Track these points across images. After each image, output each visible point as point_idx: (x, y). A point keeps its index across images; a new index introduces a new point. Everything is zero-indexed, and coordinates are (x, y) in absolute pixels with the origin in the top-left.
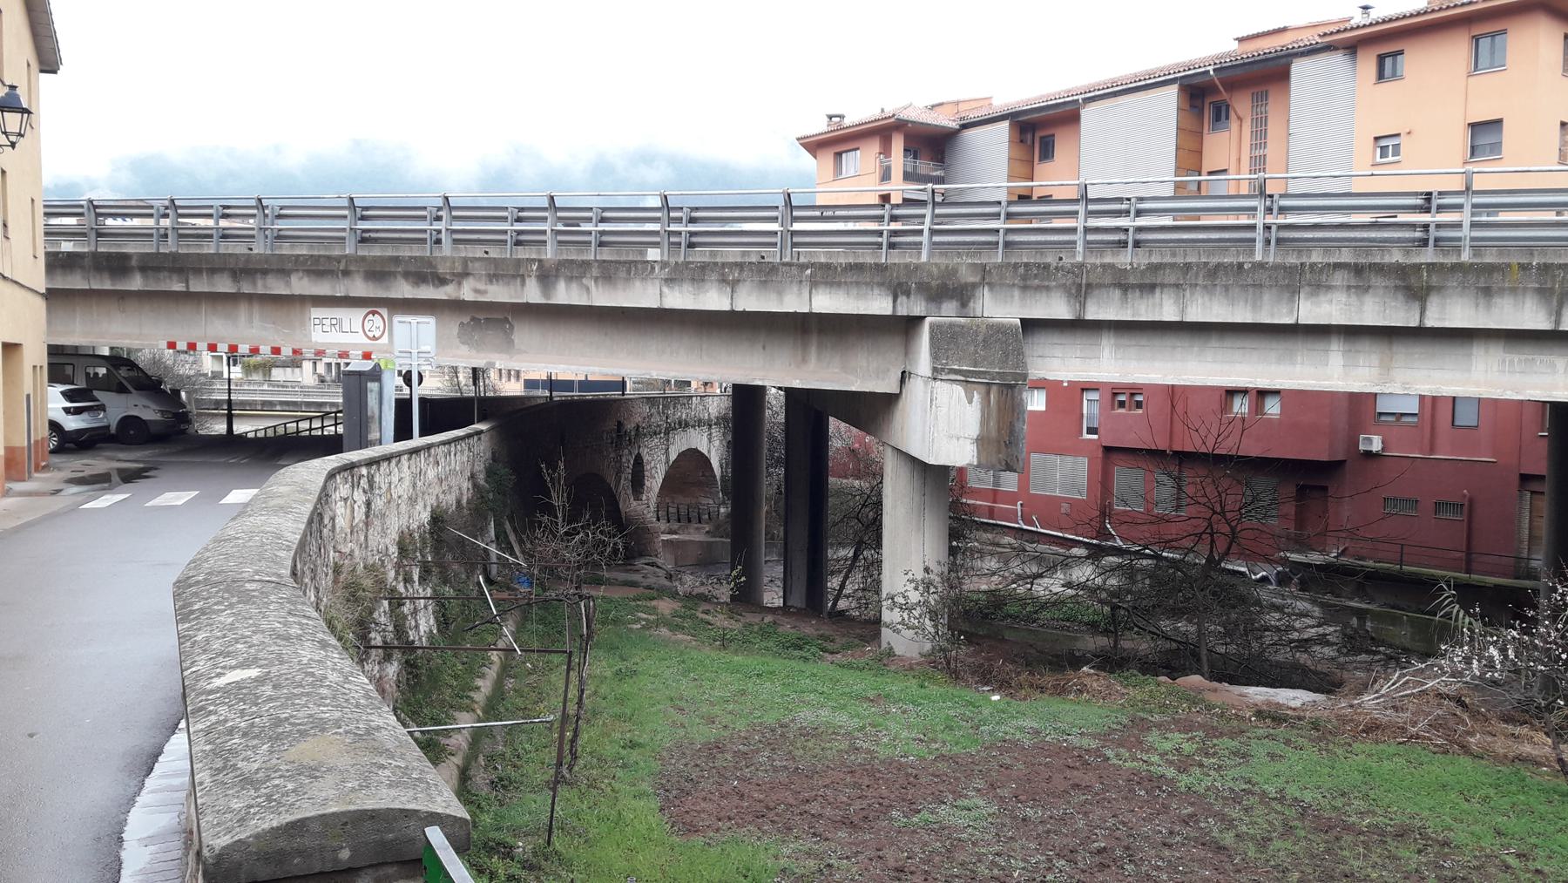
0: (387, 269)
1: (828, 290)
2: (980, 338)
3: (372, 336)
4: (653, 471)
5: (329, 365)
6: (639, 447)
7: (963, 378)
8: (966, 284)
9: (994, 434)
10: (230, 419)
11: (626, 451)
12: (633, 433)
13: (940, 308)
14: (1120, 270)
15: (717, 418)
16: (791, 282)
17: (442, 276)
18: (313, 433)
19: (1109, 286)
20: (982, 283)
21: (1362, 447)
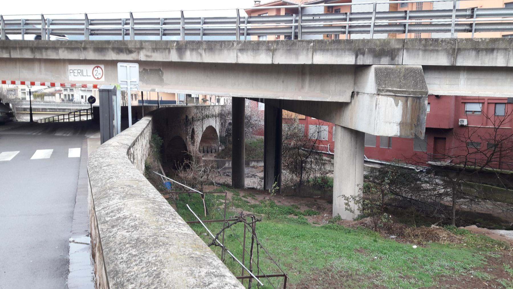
0: (104, 47)
1: (322, 53)
2: (402, 75)
3: (97, 78)
5: (65, 95)
6: (193, 125)
7: (393, 94)
8: (394, 49)
9: (409, 121)
10: (31, 115)
11: (189, 127)
12: (191, 120)
13: (380, 61)
14: (476, 42)
15: (218, 114)
16: (303, 49)
17: (130, 49)
18: (65, 120)
19: (469, 50)
20: (403, 48)
21: (460, 124)
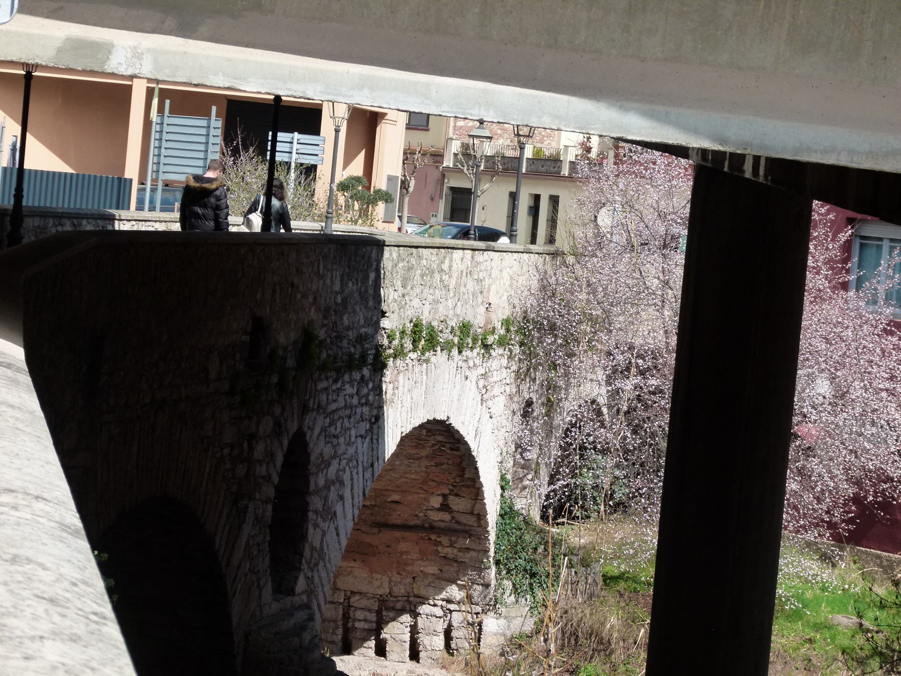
4: (333, 496)
11: (267, 424)
15: (507, 323)
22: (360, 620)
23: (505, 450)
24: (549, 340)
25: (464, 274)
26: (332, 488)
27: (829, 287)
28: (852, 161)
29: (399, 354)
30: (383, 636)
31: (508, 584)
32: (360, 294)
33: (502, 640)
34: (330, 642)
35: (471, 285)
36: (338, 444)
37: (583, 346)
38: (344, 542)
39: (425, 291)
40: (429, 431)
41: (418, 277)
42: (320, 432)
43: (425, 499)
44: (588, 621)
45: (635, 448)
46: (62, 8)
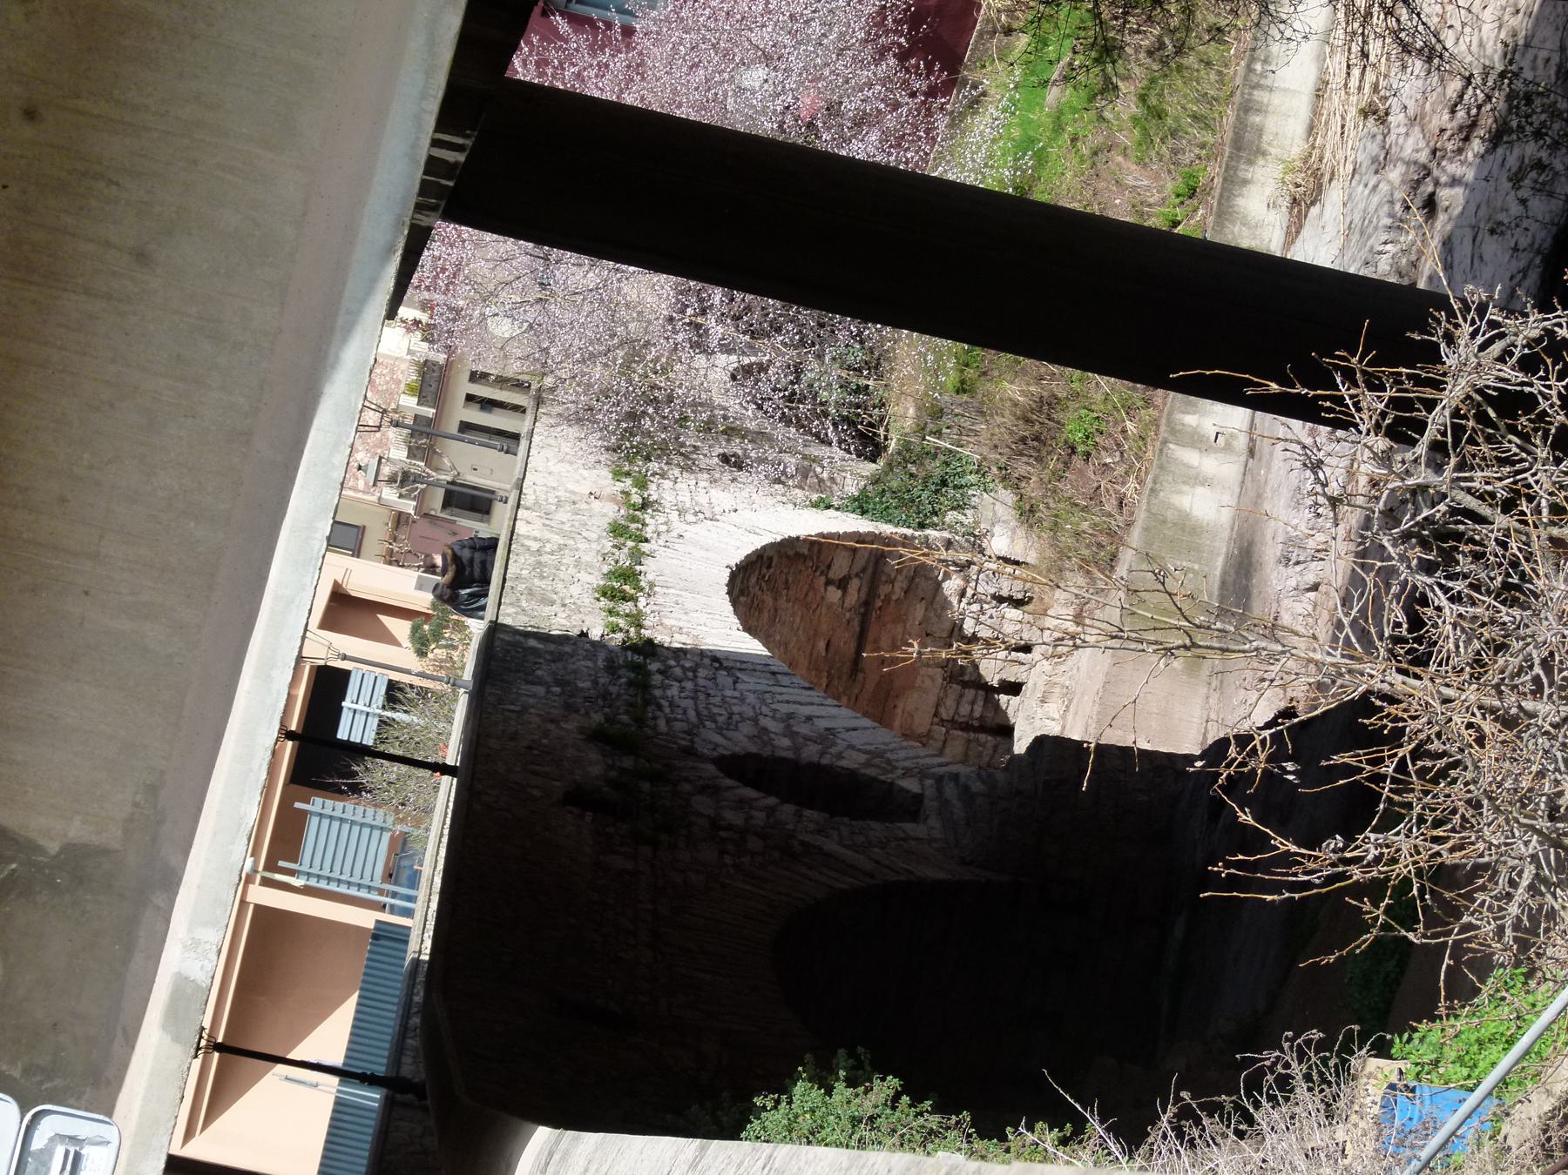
4: (804, 729)
11: (702, 803)
15: (618, 474)
22: (972, 710)
23: (779, 498)
24: (647, 423)
25: (547, 522)
26: (795, 729)
27: (627, 53)
28: (435, 97)
29: (637, 620)
30: (995, 684)
31: (951, 516)
32: (554, 662)
33: (1021, 532)
34: (995, 751)
35: (563, 515)
36: (740, 714)
37: (660, 381)
38: (866, 722)
39: (562, 577)
40: (742, 593)
41: (543, 584)
42: (723, 735)
43: (829, 607)
44: (1008, 420)
45: (800, 332)
46: (125, 1032)
